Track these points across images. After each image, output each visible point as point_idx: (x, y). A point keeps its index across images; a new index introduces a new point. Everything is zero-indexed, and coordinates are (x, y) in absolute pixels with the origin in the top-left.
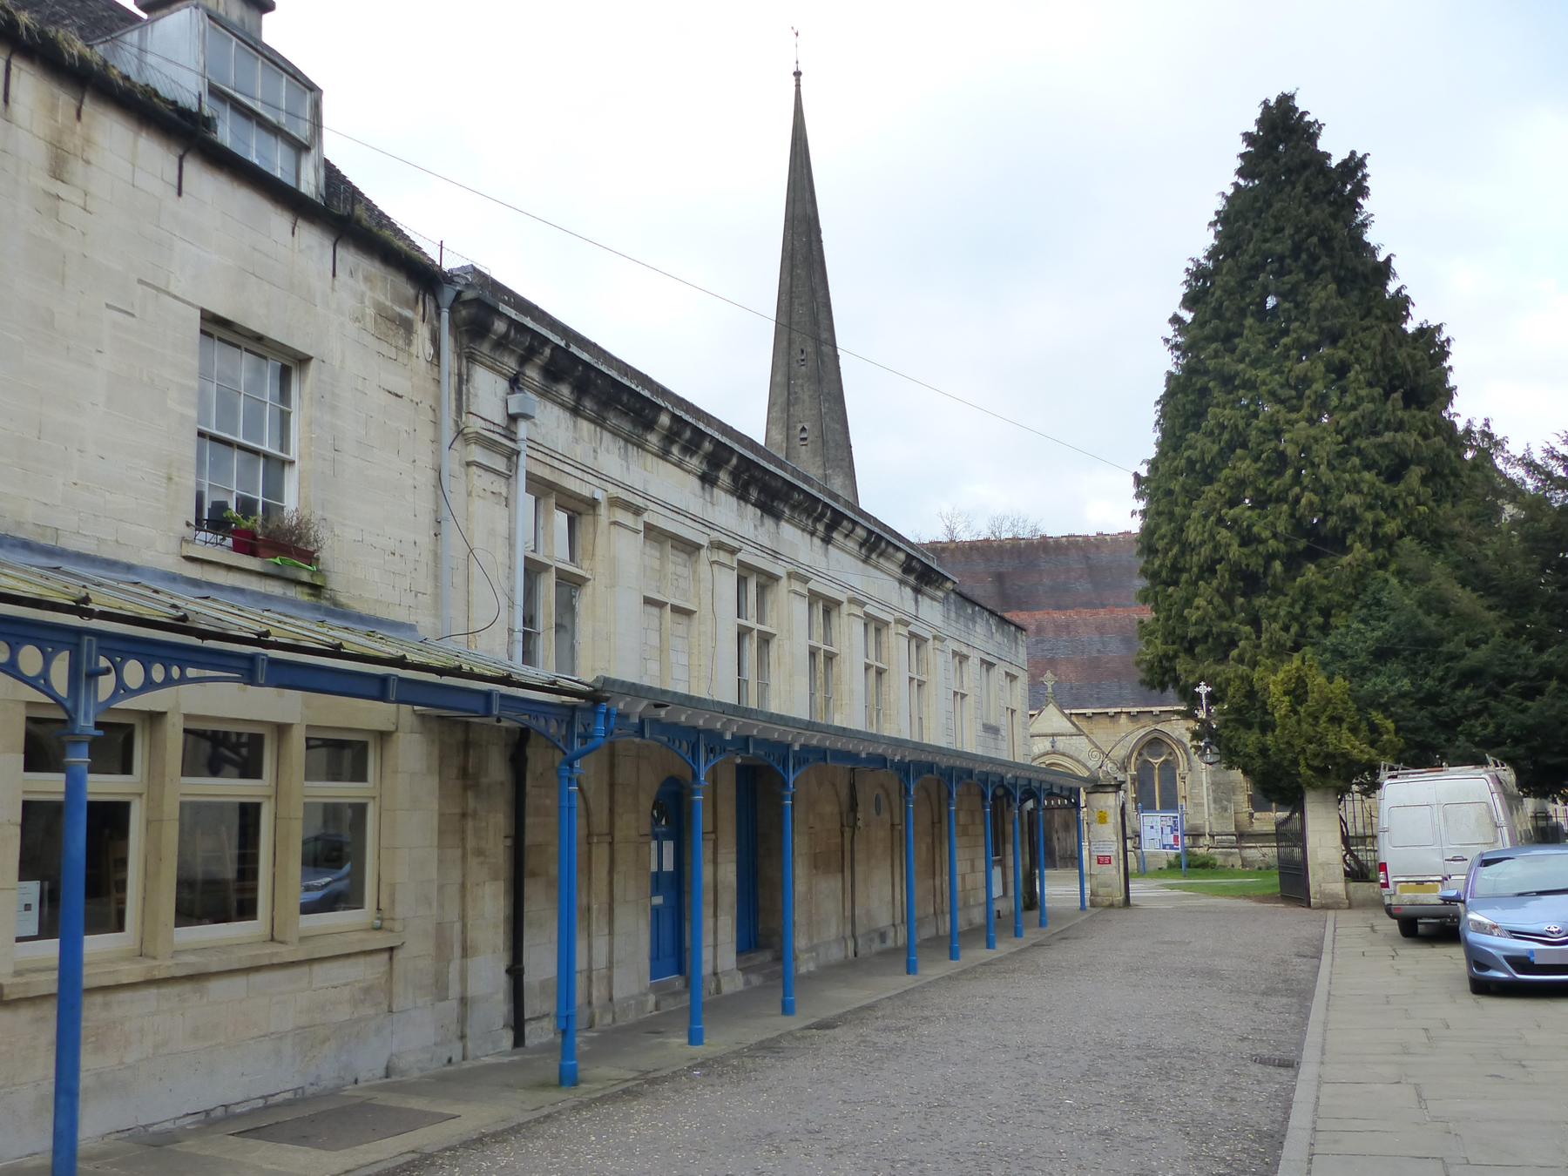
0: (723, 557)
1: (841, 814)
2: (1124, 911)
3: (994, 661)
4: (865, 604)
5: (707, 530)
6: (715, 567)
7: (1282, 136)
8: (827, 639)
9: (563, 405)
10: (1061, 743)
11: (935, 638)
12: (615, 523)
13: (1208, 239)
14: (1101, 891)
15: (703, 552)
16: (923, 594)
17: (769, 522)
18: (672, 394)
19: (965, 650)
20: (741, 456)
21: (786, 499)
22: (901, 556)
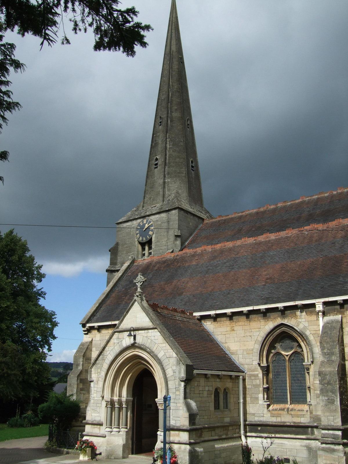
10: (141, 338)
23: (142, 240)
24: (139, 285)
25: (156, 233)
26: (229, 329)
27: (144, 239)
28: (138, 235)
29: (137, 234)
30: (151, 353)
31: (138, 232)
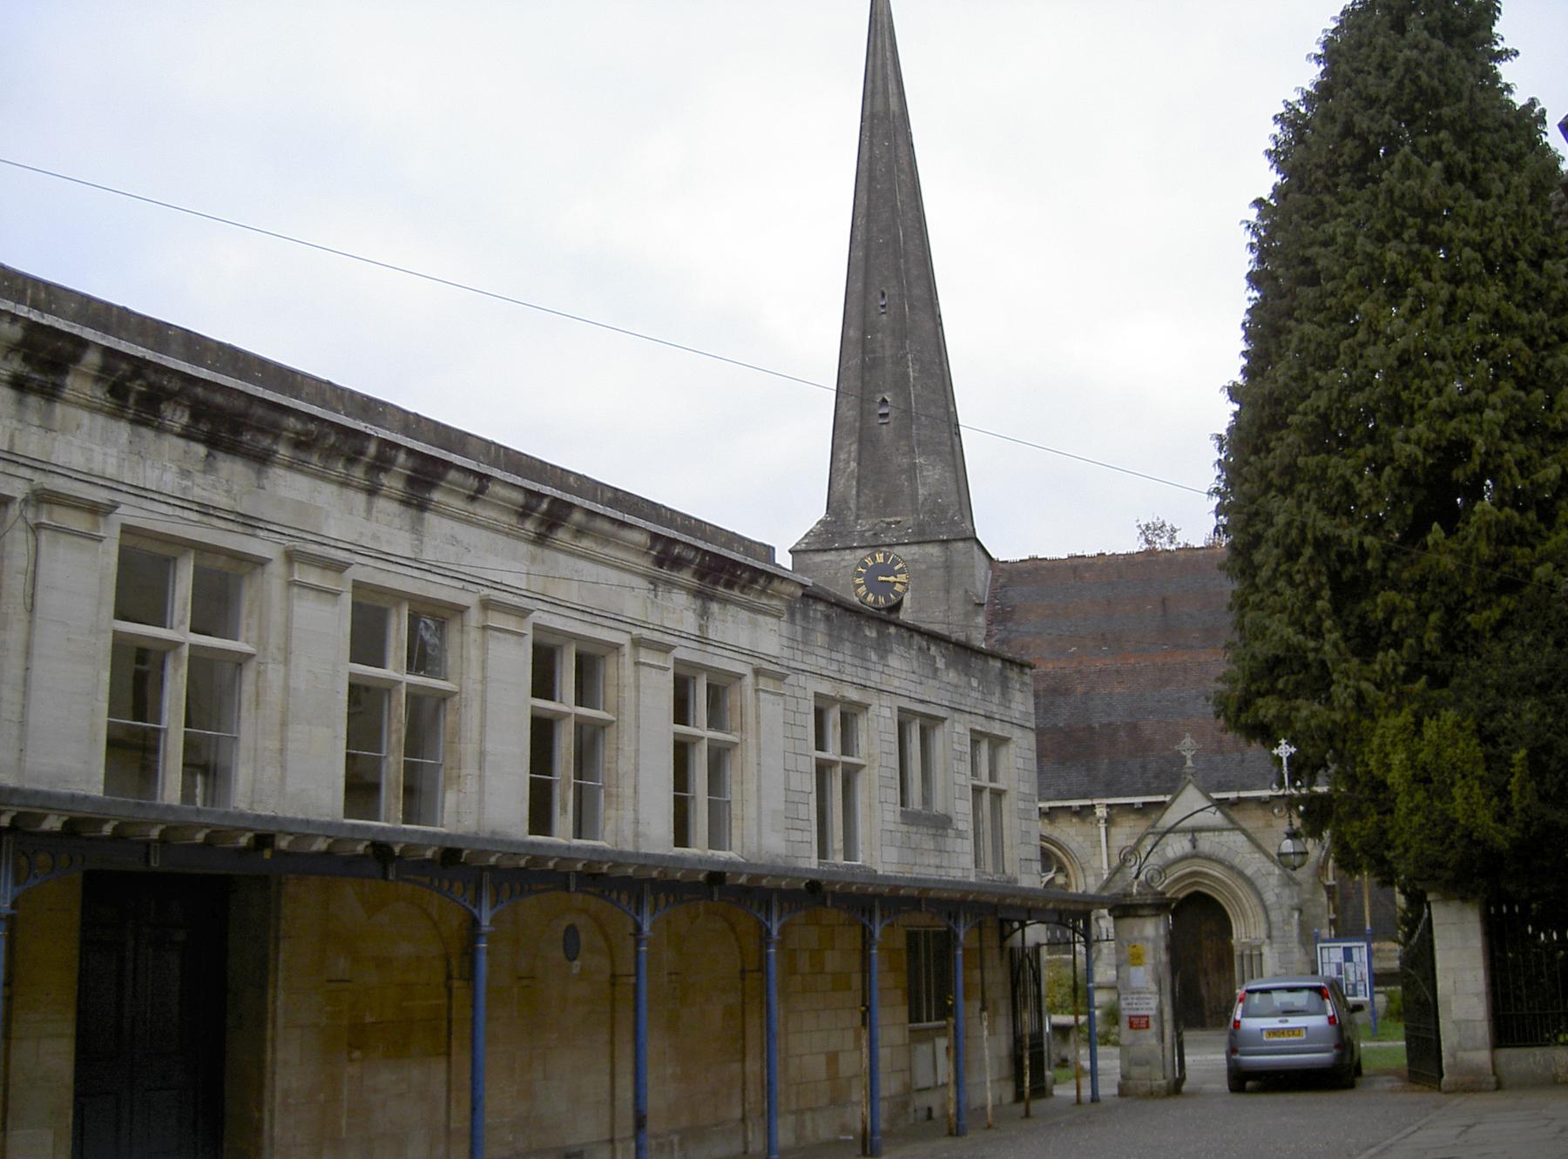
0: (510, 623)
1: (447, 959)
2: (1173, 1101)
3: (941, 713)
4: (113, 507)
5: (749, 659)
6: (295, 590)
7: (1517, 53)
8: (847, 747)
9: (359, 488)
10: (1207, 843)
11: (758, 672)
12: (292, 583)
13: (1311, 74)
14: (1136, 1072)
15: (14, 510)
16: (712, 598)
17: (233, 470)
18: (263, 363)
19: (996, 729)
20: (411, 452)
21: (275, 431)
22: (642, 539)
23: (876, 601)
24: (1188, 755)
25: (914, 590)
26: (1261, 823)
27: (882, 600)
28: (863, 588)
29: (860, 585)
30: (1231, 868)
31: (859, 581)
